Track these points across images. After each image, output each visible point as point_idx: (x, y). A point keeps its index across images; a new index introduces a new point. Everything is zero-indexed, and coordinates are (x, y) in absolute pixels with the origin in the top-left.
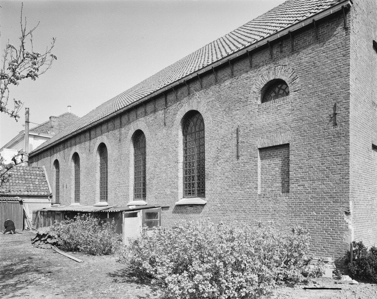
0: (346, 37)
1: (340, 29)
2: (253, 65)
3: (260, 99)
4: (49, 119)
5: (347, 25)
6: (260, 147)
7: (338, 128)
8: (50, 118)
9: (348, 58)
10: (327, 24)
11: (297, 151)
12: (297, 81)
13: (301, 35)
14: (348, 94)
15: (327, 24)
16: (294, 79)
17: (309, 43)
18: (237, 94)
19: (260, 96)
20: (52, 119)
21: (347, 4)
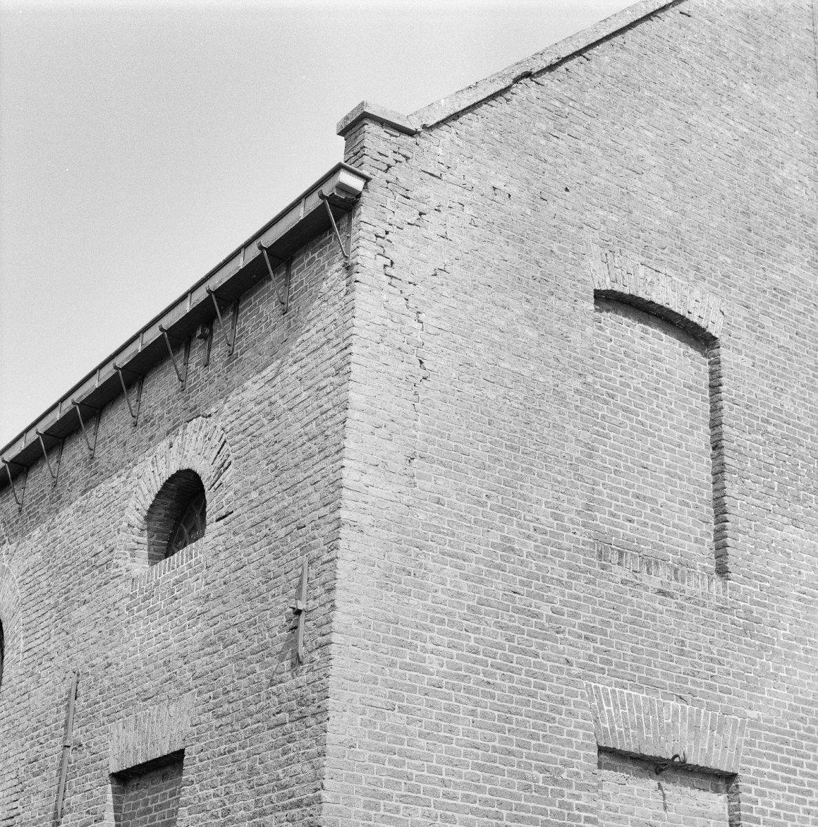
0: (348, 298)
1: (334, 271)
2: (141, 419)
3: (144, 553)
4: (336, 150)
5: (352, 255)
6: (115, 768)
7: (304, 677)
8: (352, 128)
9: (346, 378)
10: (310, 257)
11: (197, 786)
12: (228, 478)
13: (252, 298)
14: (335, 525)
15: (310, 257)
16: (223, 467)
17: (267, 325)
18: (92, 535)
19: (144, 539)
20: (373, 136)
21: (335, 184)
